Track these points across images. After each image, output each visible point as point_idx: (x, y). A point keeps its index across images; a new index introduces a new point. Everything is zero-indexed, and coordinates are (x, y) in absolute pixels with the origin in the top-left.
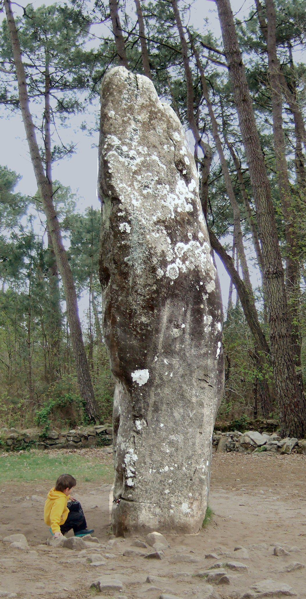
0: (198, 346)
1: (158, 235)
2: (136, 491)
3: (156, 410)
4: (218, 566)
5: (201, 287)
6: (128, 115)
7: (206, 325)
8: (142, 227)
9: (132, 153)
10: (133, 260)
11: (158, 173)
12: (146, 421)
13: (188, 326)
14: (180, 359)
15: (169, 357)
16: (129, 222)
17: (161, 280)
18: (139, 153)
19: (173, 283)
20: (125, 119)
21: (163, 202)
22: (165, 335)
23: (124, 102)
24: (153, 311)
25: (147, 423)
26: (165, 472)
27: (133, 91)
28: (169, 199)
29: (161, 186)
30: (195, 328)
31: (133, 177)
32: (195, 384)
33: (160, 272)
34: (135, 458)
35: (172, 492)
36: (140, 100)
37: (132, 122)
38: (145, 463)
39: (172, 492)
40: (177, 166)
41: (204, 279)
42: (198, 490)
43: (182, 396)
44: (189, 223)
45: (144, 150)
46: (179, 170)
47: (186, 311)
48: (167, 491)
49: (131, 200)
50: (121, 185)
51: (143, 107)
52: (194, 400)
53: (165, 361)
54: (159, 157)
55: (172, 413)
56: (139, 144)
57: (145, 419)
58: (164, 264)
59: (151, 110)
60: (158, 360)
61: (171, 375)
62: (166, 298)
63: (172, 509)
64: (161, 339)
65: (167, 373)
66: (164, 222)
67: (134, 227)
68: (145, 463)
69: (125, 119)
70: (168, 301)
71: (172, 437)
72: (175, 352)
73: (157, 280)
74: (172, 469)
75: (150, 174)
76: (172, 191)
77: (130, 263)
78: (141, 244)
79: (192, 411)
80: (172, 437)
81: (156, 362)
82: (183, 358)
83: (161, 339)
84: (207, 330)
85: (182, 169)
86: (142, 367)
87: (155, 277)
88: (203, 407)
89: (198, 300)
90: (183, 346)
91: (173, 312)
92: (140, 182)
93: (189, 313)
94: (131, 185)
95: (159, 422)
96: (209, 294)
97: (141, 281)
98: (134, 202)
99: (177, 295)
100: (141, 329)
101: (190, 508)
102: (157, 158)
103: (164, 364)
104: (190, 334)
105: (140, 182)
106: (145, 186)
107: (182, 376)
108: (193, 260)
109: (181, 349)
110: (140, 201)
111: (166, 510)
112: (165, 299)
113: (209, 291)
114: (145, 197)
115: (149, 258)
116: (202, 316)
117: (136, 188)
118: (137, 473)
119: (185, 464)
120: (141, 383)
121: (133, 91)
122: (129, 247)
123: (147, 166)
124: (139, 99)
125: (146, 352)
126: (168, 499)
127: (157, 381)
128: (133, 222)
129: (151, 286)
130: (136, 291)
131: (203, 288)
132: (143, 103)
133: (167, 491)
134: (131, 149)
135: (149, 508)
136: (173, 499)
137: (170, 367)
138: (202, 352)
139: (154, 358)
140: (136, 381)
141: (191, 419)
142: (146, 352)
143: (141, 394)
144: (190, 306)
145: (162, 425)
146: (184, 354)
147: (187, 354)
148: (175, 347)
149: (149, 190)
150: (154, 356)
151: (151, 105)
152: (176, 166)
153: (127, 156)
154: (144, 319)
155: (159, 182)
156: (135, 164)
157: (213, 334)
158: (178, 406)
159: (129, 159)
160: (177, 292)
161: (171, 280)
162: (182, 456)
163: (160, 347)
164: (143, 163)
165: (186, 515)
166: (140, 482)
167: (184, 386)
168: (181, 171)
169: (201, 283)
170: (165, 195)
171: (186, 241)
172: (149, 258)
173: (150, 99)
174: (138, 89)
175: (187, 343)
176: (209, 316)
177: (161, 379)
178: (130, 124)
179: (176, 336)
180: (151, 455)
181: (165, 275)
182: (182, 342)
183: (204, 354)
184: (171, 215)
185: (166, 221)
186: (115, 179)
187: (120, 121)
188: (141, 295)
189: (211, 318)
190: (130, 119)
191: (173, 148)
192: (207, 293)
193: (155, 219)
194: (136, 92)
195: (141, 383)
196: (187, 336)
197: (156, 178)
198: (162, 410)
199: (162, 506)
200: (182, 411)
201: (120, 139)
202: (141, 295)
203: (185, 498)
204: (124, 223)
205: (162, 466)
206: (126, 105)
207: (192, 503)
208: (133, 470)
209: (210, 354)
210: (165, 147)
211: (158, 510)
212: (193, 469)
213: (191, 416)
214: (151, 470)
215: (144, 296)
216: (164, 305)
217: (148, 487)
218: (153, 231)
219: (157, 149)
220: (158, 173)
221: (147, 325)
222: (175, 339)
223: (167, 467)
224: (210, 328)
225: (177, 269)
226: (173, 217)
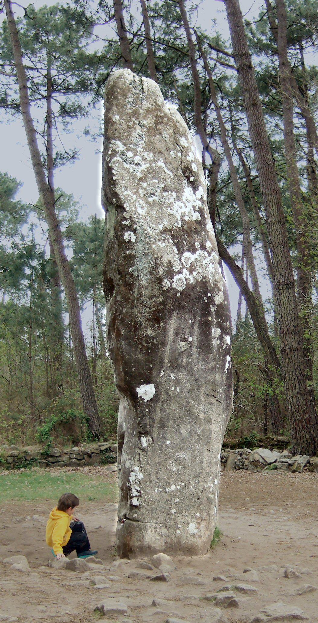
0: (206, 360)
1: (164, 244)
2: (142, 510)
3: (163, 426)
5: (209, 298)
6: (133, 119)
7: (214, 338)
8: (147, 236)
9: (137, 159)
10: (139, 270)
11: (164, 180)
12: (152, 438)
13: (195, 339)
14: (187, 373)
15: (175, 371)
16: (134, 231)
17: (168, 291)
18: (144, 159)
19: (179, 294)
20: (130, 124)
21: (169, 210)
22: (171, 348)
23: (129, 106)
24: (159, 324)
25: (153, 440)
26: (172, 491)
27: (139, 94)
28: (176, 207)
29: (167, 193)
30: (202, 341)
31: (138, 184)
32: (203, 399)
33: (166, 283)
34: (141, 476)
35: (179, 512)
36: (146, 104)
37: (137, 127)
38: (151, 482)
39: (179, 512)
40: (184, 172)
41: (212, 291)
42: (205, 510)
43: (190, 412)
44: (196, 232)
45: (149, 156)
46: (186, 177)
47: (193, 324)
48: (173, 511)
49: (136, 208)
50: (126, 193)
51: (148, 111)
52: (202, 416)
53: (172, 376)
54: (166, 163)
55: (179, 430)
56: (145, 149)
57: (150, 435)
58: (170, 274)
59: (157, 115)
60: (164, 374)
61: (178, 390)
62: (172, 310)
63: (178, 529)
64: (168, 353)
65: (173, 388)
66: (170, 231)
67: (140, 236)
68: (151, 482)
69: (130, 124)
70: (175, 313)
71: (179, 455)
72: (182, 367)
73: (164, 291)
74: (179, 487)
75: (156, 181)
76: (179, 198)
77: (135, 274)
78: (146, 254)
79: (199, 427)
80: (179, 455)
81: (162, 376)
82: (190, 372)
83: (168, 353)
84: (215, 343)
85: (189, 176)
86: (148, 382)
87: (161, 288)
88: (211, 423)
89: (206, 312)
90: (190, 360)
91: (180, 324)
92: (145, 189)
93: (196, 326)
94: (137, 193)
95: (166, 439)
96: (217, 306)
97: (146, 293)
98: (139, 210)
99: (183, 307)
100: (147, 343)
101: (197, 528)
102: (163, 165)
103: (170, 379)
104: (197, 348)
105: (145, 189)
106: (151, 194)
107: (190, 391)
108: (201, 271)
109: (188, 363)
110: (146, 209)
111: (173, 530)
112: (171, 311)
113: (217, 303)
114: (150, 205)
115: (155, 268)
116: (210, 329)
117: (142, 195)
118: (142, 492)
119: (192, 483)
120: (147, 398)
121: (139, 94)
122: (135, 257)
123: (152, 172)
124: (144, 103)
125: (151, 366)
126: (175, 519)
127: (163, 396)
128: (138, 231)
129: (157, 297)
131: (211, 300)
132: (149, 108)
133: (173, 511)
134: (137, 155)
135: (155, 528)
136: (180, 519)
137: (177, 382)
138: (210, 366)
139: (160, 373)
140: (141, 397)
141: (199, 436)
142: (151, 366)
143: (147, 410)
144: (197, 318)
145: (168, 442)
146: (191, 368)
147: (195, 369)
148: (182, 361)
149: (155, 198)
150: (160, 370)
151: (157, 109)
152: (183, 172)
153: (132, 162)
154: (149, 332)
155: (165, 190)
156: (140, 171)
157: (221, 347)
158: (185, 422)
159: (134, 166)
160: (184, 303)
161: (178, 291)
162: (189, 475)
163: (166, 361)
164: (148, 169)
165: (194, 535)
166: (145, 501)
167: (192, 402)
168: (188, 178)
169: (209, 295)
170: (172, 202)
171: (193, 250)
172: (155, 268)
173: (155, 102)
174: (143, 92)
175: (195, 357)
176: (217, 329)
177: (168, 394)
178: (135, 129)
179: (183, 350)
180: (157, 473)
181: (171, 286)
182: (189, 355)
183: (212, 368)
184: (178, 223)
185: (172, 229)
186: (119, 186)
187: (125, 126)
188: (147, 307)
189: (219, 331)
190: (135, 123)
191: (179, 154)
192: (215, 305)
193: (161, 227)
194: (141, 96)
195: (147, 398)
196: (194, 350)
197: (163, 185)
198: (168, 427)
199: (168, 526)
200: (189, 427)
201: (125, 145)
202: (147, 307)
203: (193, 518)
204: (129, 232)
205: (168, 484)
206: (131, 109)
207: (200, 523)
208: (138, 489)
209: (218, 368)
210: (172, 153)
211: (164, 531)
212: (201, 488)
213: (199, 432)
214: (157, 489)
215: (150, 308)
216: (170, 317)
217: (154, 506)
218: (159, 240)
219: (163, 155)
220: (164, 180)
221: (153, 338)
222: (182, 352)
223: (173, 486)
224: (218, 342)
225: (184, 280)
226: (180, 226)
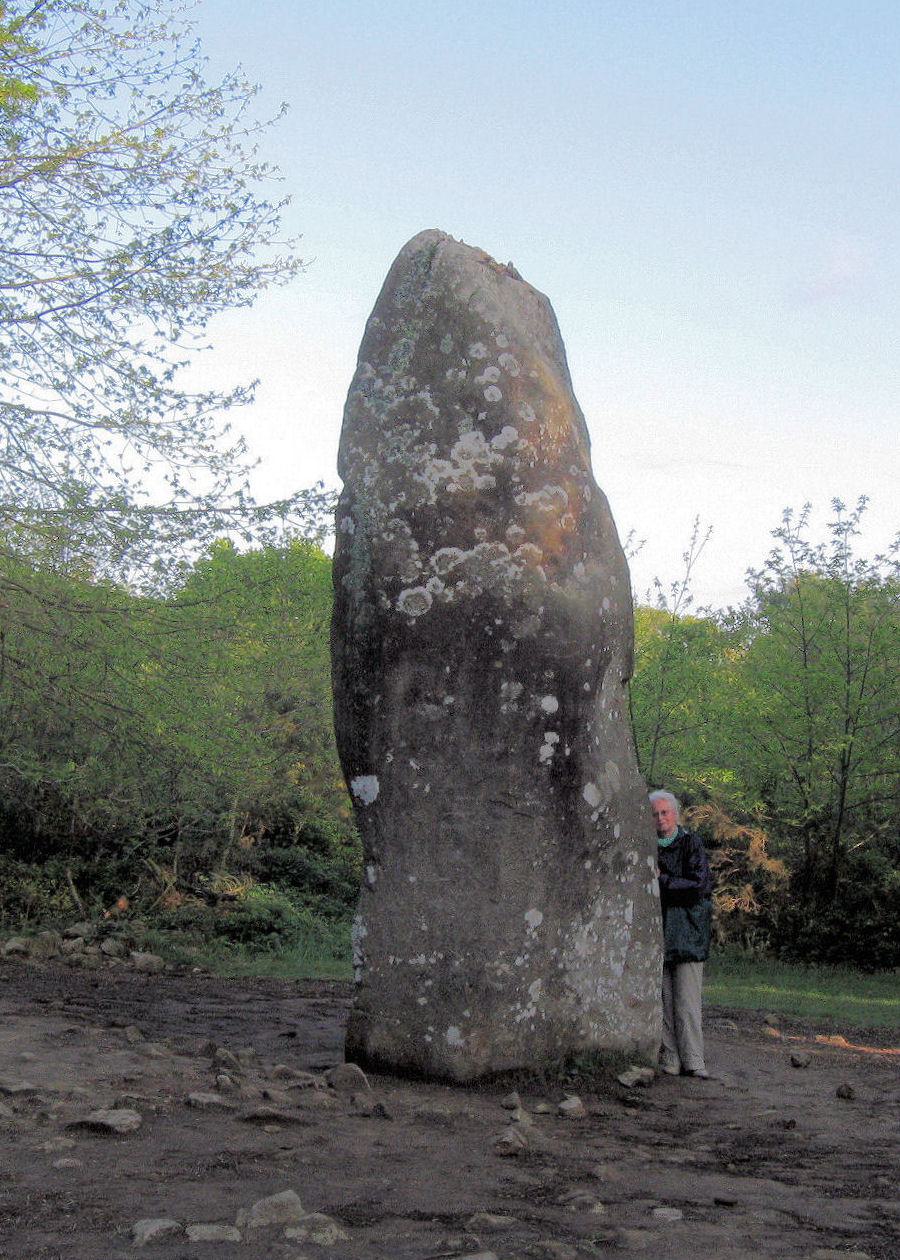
13: (462, 701)
53: (412, 763)
76: (442, 454)
131: (503, 632)
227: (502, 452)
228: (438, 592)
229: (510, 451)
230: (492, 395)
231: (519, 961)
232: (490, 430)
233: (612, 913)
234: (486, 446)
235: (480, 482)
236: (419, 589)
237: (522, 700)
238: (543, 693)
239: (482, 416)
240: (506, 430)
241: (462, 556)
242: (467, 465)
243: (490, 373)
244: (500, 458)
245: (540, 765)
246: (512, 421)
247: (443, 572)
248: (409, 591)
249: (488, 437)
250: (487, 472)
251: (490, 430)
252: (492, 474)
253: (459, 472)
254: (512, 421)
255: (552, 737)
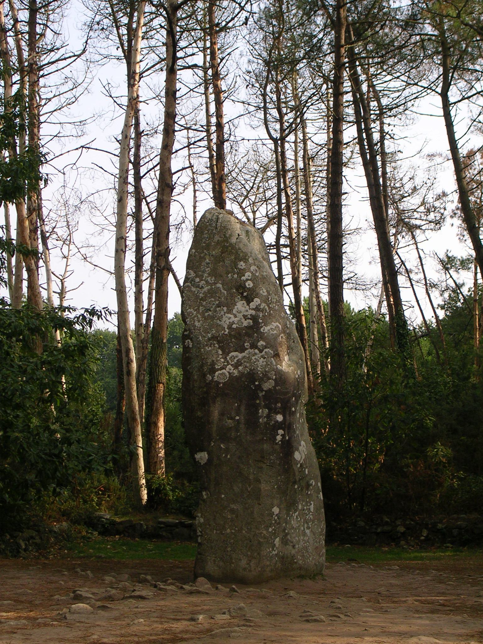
1: (210, 348)
4: (46, 617)
5: (256, 386)
7: (261, 417)
8: (199, 343)
11: (219, 298)
18: (207, 282)
19: (221, 385)
21: (218, 322)
23: (204, 240)
27: (212, 230)
31: (200, 303)
33: (209, 377)
34: (202, 520)
36: (217, 238)
37: (207, 257)
38: (210, 525)
40: (237, 290)
45: (211, 280)
47: (239, 406)
49: (194, 322)
50: (189, 310)
51: (218, 243)
52: (251, 477)
53: (222, 446)
54: (223, 285)
58: (213, 371)
59: (224, 245)
64: (215, 429)
65: (224, 455)
66: (217, 337)
68: (210, 525)
71: (232, 506)
74: (233, 531)
75: (213, 299)
76: (230, 311)
77: (191, 370)
78: (197, 356)
79: (250, 486)
80: (232, 506)
83: (215, 429)
86: (202, 450)
88: (260, 483)
89: (253, 395)
91: (224, 407)
92: (204, 306)
93: (243, 409)
96: (266, 391)
97: (197, 384)
98: (197, 324)
101: (248, 564)
102: (220, 286)
105: (204, 306)
106: (208, 310)
108: (248, 365)
115: (202, 366)
117: (201, 311)
120: (202, 463)
121: (212, 230)
123: (212, 293)
124: (216, 236)
126: (230, 556)
128: (193, 339)
130: (194, 392)
131: (259, 387)
133: (229, 549)
135: (214, 561)
138: (258, 438)
140: (198, 461)
141: (249, 492)
145: (223, 496)
147: (244, 440)
148: (231, 435)
149: (210, 313)
151: (224, 241)
153: (198, 286)
154: (199, 413)
155: (218, 306)
157: (269, 424)
159: (198, 289)
161: (220, 383)
163: (214, 435)
164: (209, 290)
165: (245, 569)
166: (206, 539)
168: (242, 294)
169: (257, 383)
171: (242, 350)
172: (202, 366)
173: (224, 235)
174: (216, 228)
182: (237, 430)
184: (225, 331)
190: (206, 254)
191: (236, 276)
194: (214, 231)
195: (202, 463)
196: (242, 426)
197: (217, 302)
200: (240, 485)
201: (195, 272)
206: (205, 243)
207: (250, 561)
210: (230, 275)
211: (221, 564)
212: (253, 533)
213: (249, 489)
216: (214, 402)
217: (213, 544)
218: (207, 345)
220: (219, 298)
224: (266, 419)
225: (227, 374)
227: (253, 309)
228: (231, 371)
229: (257, 309)
230: (249, 285)
231: (270, 530)
232: (249, 300)
233: (305, 508)
234: (248, 307)
235: (245, 323)
236: (224, 371)
237: (268, 416)
238: (277, 413)
239: (245, 294)
240: (256, 299)
241: (240, 356)
242: (240, 316)
243: (248, 275)
244: (253, 312)
245: (277, 444)
246: (257, 295)
247: (233, 363)
248: (220, 372)
249: (248, 304)
250: (249, 319)
251: (249, 300)
252: (250, 319)
253: (236, 320)
254: (257, 295)
255: (281, 432)
